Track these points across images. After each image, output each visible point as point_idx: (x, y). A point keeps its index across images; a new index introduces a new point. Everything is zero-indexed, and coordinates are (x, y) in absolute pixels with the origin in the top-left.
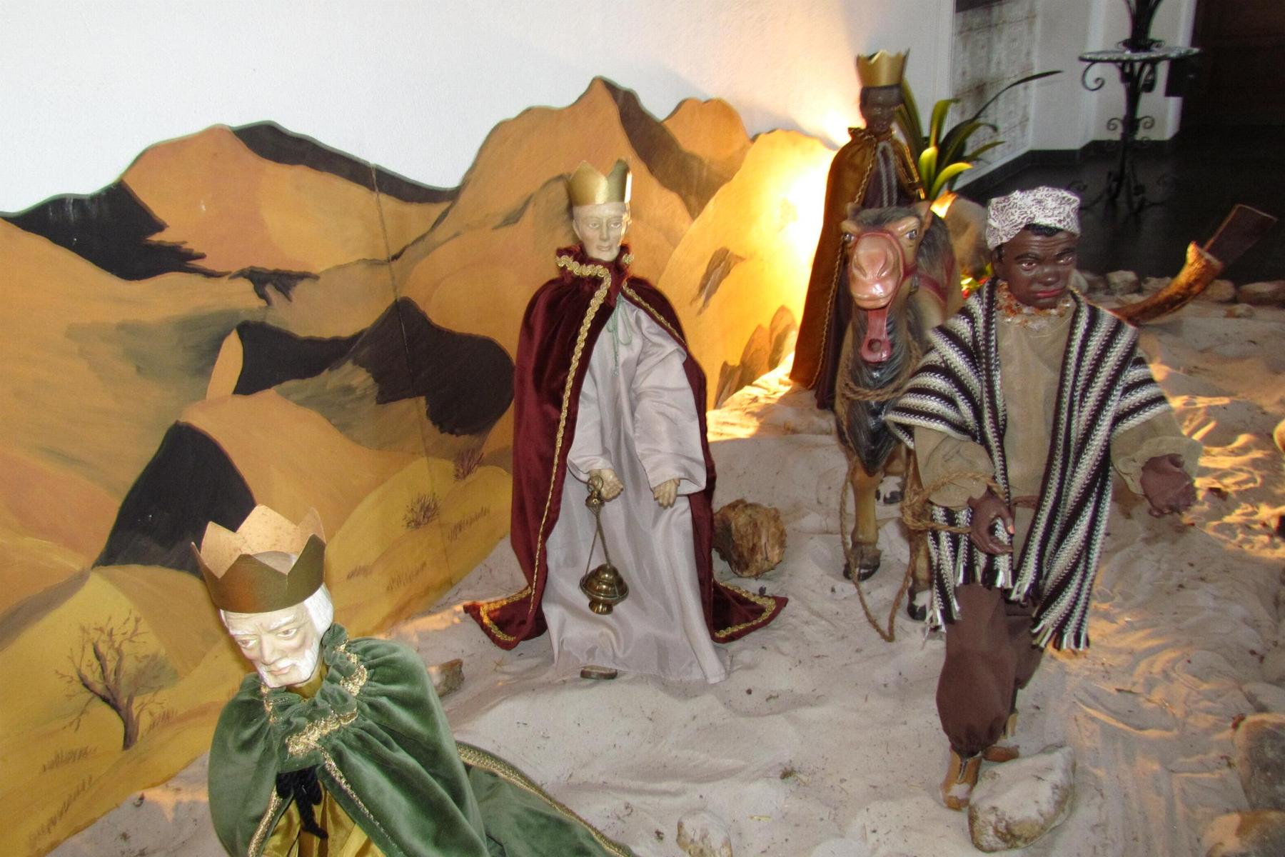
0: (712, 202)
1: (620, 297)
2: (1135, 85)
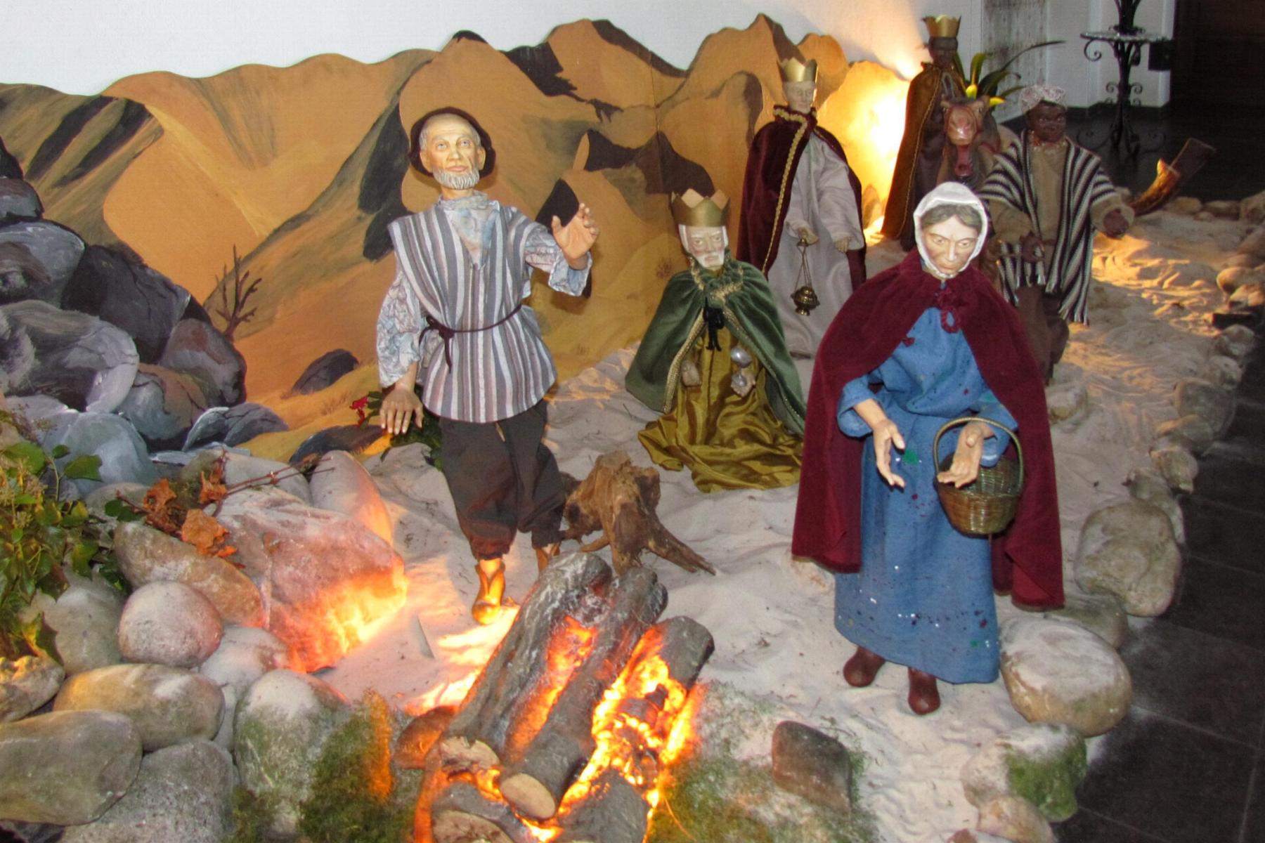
0: (826, 103)
1: (812, 134)
2: (1126, 60)
